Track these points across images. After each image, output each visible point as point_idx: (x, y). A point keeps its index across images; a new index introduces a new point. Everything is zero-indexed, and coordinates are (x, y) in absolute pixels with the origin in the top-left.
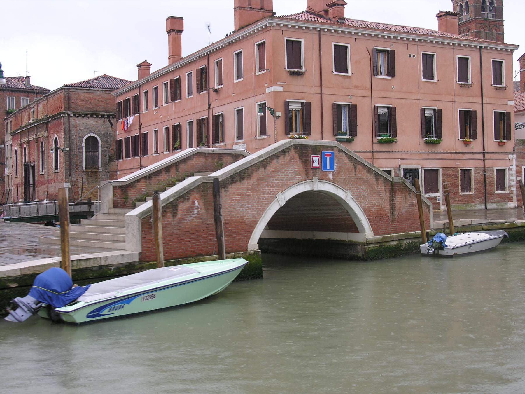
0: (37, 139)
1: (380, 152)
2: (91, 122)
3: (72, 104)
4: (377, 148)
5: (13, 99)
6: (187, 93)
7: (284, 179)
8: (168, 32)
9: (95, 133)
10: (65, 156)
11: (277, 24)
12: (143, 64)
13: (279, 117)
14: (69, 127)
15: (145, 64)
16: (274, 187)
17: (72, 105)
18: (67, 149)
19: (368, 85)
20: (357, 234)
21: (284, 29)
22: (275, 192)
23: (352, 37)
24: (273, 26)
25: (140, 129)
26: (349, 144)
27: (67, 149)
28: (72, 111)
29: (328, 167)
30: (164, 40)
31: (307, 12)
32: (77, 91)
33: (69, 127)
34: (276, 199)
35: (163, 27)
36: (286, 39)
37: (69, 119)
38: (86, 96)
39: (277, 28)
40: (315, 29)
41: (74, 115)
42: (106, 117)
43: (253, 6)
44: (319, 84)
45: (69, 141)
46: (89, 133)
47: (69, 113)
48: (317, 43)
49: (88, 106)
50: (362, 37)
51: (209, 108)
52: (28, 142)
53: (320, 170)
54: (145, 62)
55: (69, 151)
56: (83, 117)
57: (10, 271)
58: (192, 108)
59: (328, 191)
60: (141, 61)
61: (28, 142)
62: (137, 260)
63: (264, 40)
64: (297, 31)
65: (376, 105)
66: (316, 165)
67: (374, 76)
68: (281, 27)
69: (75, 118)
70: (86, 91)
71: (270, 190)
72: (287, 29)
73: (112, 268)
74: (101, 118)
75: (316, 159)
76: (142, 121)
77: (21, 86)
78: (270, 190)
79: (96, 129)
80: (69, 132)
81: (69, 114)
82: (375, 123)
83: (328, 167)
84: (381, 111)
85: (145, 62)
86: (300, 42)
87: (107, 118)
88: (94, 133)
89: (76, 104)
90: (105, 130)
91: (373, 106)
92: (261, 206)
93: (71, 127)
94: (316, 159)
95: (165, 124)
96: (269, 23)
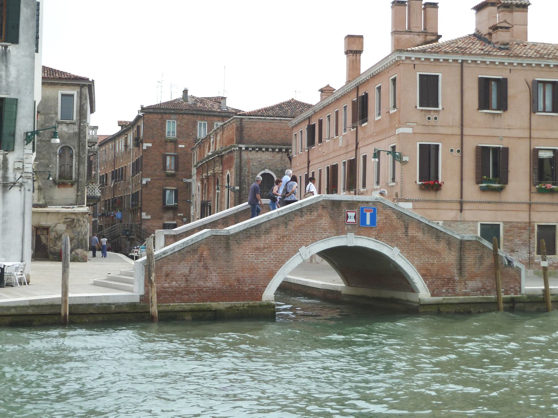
0: (214, 175)
1: (539, 203)
2: (267, 156)
3: (244, 135)
4: (537, 198)
5: (205, 124)
6: (343, 129)
7: (309, 234)
8: (347, 53)
9: (271, 170)
10: (235, 196)
11: (406, 58)
12: (325, 89)
13: (406, 162)
14: (241, 162)
15: (327, 89)
16: (297, 241)
17: (246, 138)
18: (237, 188)
19: (526, 125)
20: (413, 293)
21: (417, 62)
22: (297, 246)
23: (505, 67)
24: (403, 60)
25: (308, 167)
26: (498, 194)
27: (237, 188)
28: (244, 143)
29: (368, 222)
30: (343, 60)
31: (474, 35)
32: (251, 120)
33: (241, 162)
34: (299, 253)
35: (341, 47)
36: (418, 73)
37: (241, 153)
38: (261, 126)
39: (408, 61)
40: (455, 61)
41: (247, 149)
42: (284, 150)
43: (413, 29)
44: (460, 123)
45: (240, 179)
46: (264, 169)
47: (240, 146)
48: (458, 77)
49: (263, 138)
50: (520, 68)
51: (357, 148)
52: (207, 178)
53: (358, 226)
54: (328, 86)
55: (240, 191)
56: (257, 151)
57: (26, 301)
58: (335, 148)
59: (367, 247)
60: (323, 86)
61: (207, 178)
62: (138, 301)
63: (396, 75)
64: (433, 64)
65: (537, 147)
66: (351, 220)
67: (534, 112)
68: (413, 61)
69: (248, 152)
70: (261, 121)
71: (291, 244)
72: (420, 63)
73: (113, 306)
74: (279, 152)
75: (351, 214)
76: (311, 158)
77: (216, 107)
78: (291, 244)
79: (272, 165)
80: (240, 169)
81: (241, 148)
82: (534, 169)
83: (368, 222)
84: (543, 155)
85: (328, 86)
86: (437, 76)
87: (285, 152)
88: (270, 169)
89: (249, 136)
90: (282, 166)
91: (532, 149)
92: (280, 259)
93: (243, 162)
94: (351, 214)
95: (326, 163)
96: (398, 57)
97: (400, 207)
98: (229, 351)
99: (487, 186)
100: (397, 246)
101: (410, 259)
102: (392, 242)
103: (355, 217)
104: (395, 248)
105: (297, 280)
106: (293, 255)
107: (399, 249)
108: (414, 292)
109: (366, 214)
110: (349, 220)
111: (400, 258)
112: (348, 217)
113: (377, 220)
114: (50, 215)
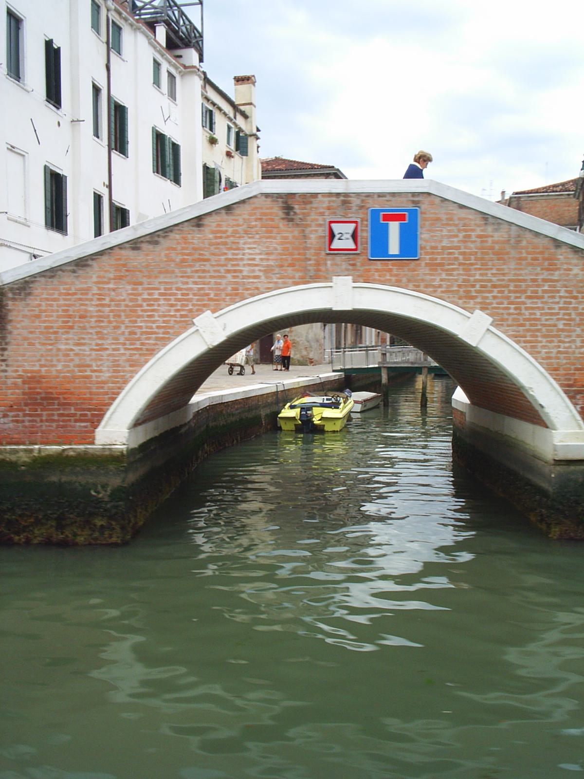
16: (190, 300)
22: (190, 311)
29: (394, 247)
71: (172, 305)
83: (394, 247)
92: (142, 344)
97: (57, 254)
98: (239, 461)
99: (174, 63)
100: (482, 309)
101: (525, 335)
102: (465, 297)
103: (354, 236)
104: (478, 312)
105: (365, 336)
106: (178, 334)
107: (490, 315)
108: (547, 427)
109: (386, 229)
110: (336, 244)
111: (494, 340)
112: (332, 236)
113: (420, 242)
114: (238, 211)
